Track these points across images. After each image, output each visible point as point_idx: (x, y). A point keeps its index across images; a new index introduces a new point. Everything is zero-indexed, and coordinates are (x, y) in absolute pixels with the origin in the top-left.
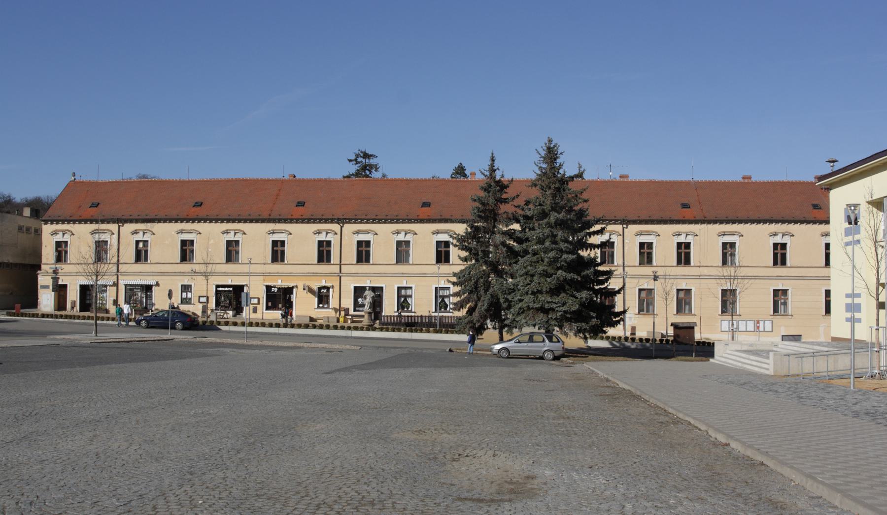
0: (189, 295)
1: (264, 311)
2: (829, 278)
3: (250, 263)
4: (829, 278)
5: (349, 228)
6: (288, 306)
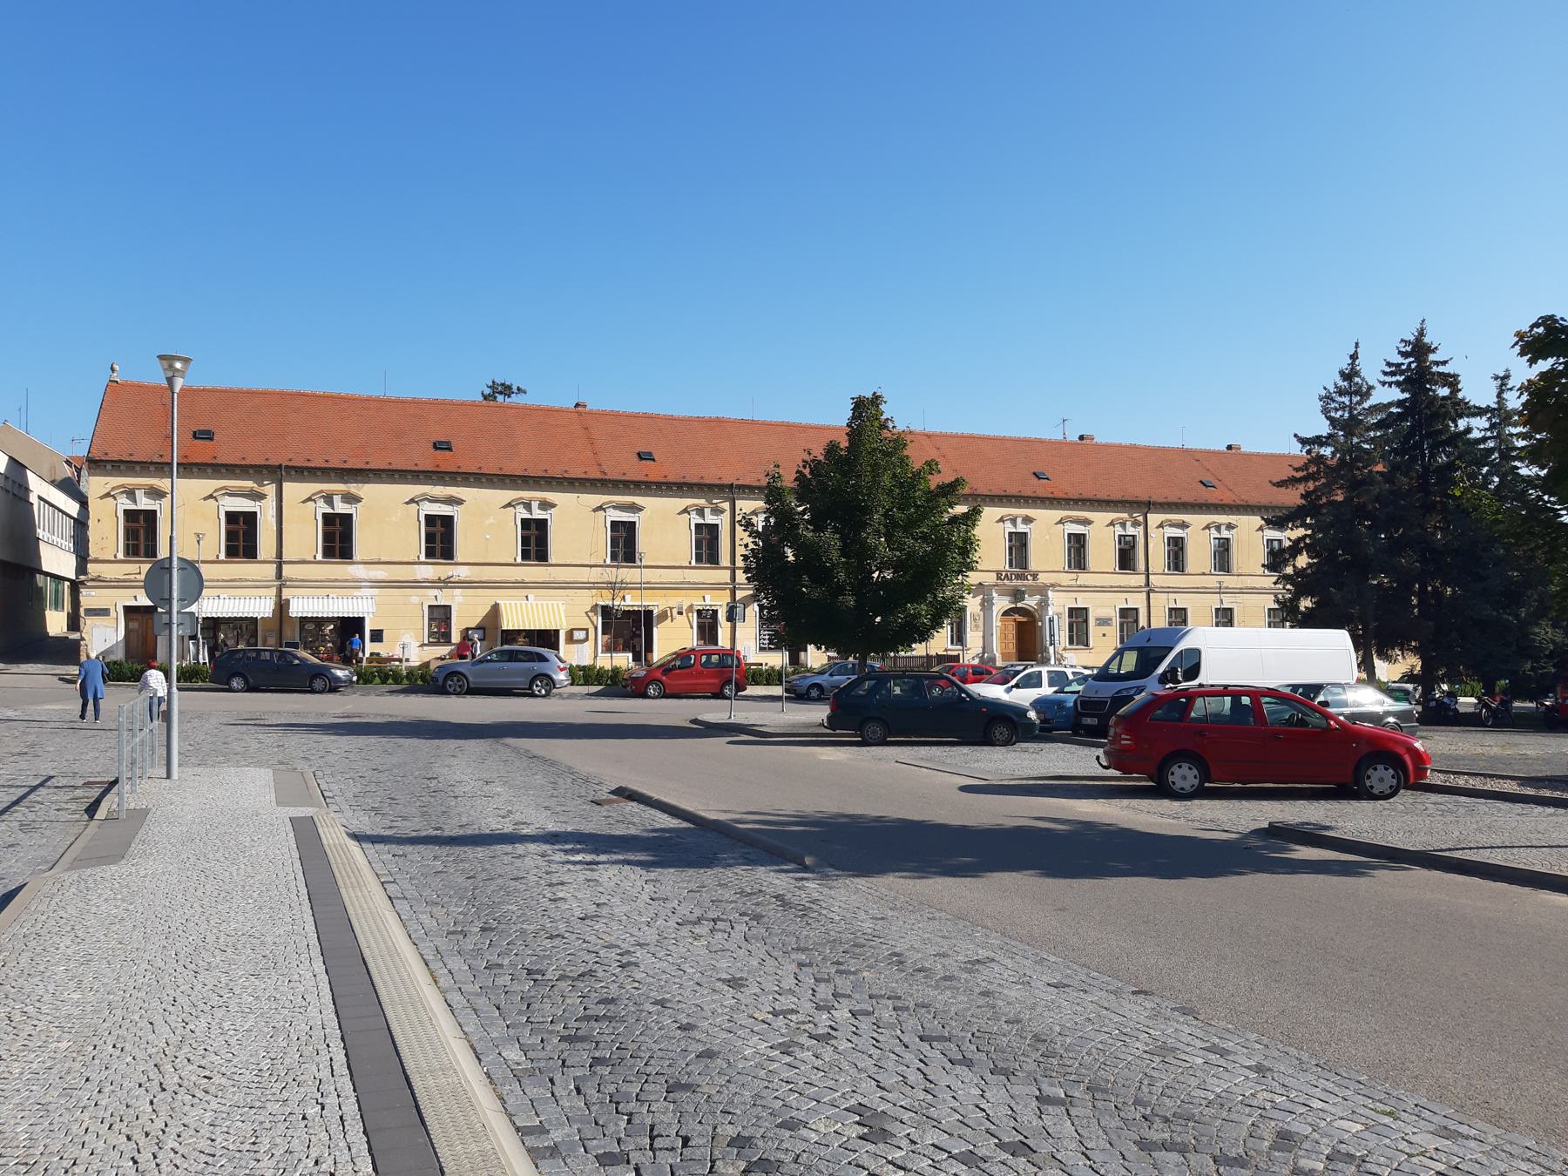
1: (600, 654)
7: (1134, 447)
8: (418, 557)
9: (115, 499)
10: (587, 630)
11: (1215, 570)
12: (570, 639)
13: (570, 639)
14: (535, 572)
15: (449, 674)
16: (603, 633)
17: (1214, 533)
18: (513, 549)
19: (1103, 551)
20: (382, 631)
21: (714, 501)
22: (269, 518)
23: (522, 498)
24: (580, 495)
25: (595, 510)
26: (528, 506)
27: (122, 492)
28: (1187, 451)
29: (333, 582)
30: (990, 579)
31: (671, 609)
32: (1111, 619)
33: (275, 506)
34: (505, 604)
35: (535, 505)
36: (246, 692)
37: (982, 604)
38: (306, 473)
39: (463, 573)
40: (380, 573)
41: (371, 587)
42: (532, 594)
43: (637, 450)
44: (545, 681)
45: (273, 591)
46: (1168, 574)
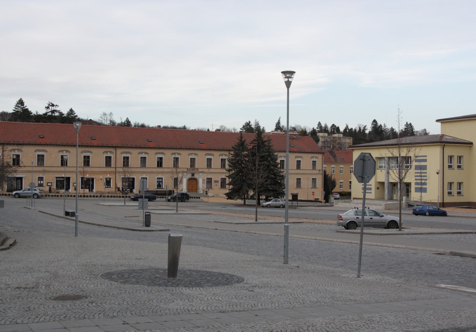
0: (42, 182)
1: (80, 189)
2: (416, 174)
3: (77, 167)
4: (416, 174)
5: (119, 151)
6: (91, 188)
18: (36, 163)
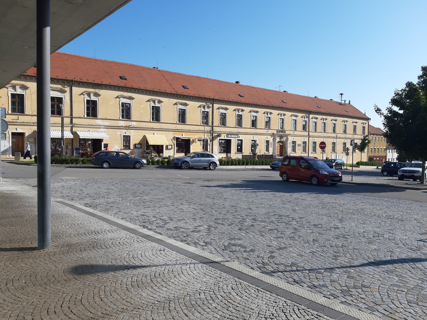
1: (175, 154)
7: (298, 95)
8: (120, 118)
9: (7, 89)
10: (172, 145)
11: (221, 124)
12: (167, 148)
13: (167, 148)
14: (156, 125)
15: (182, 162)
16: (176, 147)
17: (237, 113)
19: (247, 122)
20: (108, 144)
21: (208, 104)
22: (67, 100)
23: (152, 99)
24: (170, 99)
25: (174, 105)
26: (154, 102)
27: (11, 86)
28: (309, 97)
29: (91, 126)
30: (275, 132)
31: (195, 139)
32: (301, 145)
33: (69, 95)
34: (148, 136)
35: (156, 101)
36: (108, 168)
37: (273, 140)
38: (81, 84)
39: (134, 124)
40: (107, 123)
41: (104, 128)
42: (156, 132)
43: (119, 75)
44: (214, 165)
45: (69, 128)
46: (220, 127)
